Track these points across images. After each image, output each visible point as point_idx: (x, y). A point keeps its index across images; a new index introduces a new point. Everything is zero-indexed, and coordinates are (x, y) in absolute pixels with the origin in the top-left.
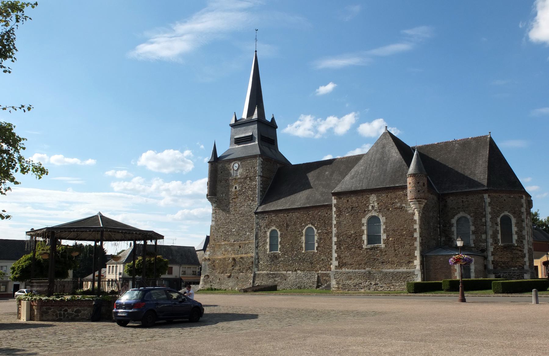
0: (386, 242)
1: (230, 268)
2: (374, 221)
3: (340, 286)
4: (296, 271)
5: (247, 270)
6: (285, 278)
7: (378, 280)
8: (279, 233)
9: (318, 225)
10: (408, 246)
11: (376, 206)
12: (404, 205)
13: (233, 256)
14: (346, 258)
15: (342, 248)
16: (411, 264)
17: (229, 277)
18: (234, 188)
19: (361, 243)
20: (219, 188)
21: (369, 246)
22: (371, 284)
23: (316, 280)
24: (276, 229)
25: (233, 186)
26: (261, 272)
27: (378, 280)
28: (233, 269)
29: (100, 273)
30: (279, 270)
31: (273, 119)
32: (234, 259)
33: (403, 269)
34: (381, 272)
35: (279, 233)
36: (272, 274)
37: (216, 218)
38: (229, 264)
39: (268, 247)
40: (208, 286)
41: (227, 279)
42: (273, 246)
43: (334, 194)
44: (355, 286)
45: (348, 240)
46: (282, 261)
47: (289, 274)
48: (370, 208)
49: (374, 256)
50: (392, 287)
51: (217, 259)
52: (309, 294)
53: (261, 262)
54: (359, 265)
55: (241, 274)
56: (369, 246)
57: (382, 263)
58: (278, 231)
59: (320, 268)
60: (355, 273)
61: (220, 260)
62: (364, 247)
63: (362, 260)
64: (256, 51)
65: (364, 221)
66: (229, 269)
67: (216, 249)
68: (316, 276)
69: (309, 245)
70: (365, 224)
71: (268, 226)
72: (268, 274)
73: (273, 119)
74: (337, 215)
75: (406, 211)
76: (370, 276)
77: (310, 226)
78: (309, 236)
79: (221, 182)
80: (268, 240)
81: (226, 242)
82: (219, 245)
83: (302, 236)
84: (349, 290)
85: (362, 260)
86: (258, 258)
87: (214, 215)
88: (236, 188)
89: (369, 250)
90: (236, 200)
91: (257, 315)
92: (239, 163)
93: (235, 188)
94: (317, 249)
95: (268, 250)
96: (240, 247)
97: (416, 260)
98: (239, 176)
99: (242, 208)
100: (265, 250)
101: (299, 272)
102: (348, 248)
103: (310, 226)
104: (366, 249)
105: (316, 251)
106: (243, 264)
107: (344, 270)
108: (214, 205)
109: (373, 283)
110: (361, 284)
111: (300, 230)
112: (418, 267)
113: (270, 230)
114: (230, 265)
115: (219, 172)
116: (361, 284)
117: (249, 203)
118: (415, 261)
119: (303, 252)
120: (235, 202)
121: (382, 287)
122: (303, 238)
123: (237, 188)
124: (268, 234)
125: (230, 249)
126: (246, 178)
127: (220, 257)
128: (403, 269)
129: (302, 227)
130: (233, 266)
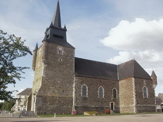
8: (87, 88)
18: (59, 60)
21: (145, 97)
25: (59, 59)
29: (159, 111)
31: (65, 27)
33: (153, 105)
35: (87, 88)
38: (56, 100)
39: (82, 93)
42: (84, 93)
53: (78, 101)
58: (87, 87)
62: (143, 97)
65: (143, 88)
67: (46, 90)
69: (101, 94)
71: (82, 83)
73: (65, 27)
78: (101, 91)
80: (82, 90)
87: (45, 71)
88: (60, 60)
91: (42, 111)
96: (63, 91)
103: (101, 87)
107: (139, 105)
108: (46, 65)
115: (49, 48)
119: (99, 97)
122: (99, 91)
123: (61, 60)
124: (82, 87)
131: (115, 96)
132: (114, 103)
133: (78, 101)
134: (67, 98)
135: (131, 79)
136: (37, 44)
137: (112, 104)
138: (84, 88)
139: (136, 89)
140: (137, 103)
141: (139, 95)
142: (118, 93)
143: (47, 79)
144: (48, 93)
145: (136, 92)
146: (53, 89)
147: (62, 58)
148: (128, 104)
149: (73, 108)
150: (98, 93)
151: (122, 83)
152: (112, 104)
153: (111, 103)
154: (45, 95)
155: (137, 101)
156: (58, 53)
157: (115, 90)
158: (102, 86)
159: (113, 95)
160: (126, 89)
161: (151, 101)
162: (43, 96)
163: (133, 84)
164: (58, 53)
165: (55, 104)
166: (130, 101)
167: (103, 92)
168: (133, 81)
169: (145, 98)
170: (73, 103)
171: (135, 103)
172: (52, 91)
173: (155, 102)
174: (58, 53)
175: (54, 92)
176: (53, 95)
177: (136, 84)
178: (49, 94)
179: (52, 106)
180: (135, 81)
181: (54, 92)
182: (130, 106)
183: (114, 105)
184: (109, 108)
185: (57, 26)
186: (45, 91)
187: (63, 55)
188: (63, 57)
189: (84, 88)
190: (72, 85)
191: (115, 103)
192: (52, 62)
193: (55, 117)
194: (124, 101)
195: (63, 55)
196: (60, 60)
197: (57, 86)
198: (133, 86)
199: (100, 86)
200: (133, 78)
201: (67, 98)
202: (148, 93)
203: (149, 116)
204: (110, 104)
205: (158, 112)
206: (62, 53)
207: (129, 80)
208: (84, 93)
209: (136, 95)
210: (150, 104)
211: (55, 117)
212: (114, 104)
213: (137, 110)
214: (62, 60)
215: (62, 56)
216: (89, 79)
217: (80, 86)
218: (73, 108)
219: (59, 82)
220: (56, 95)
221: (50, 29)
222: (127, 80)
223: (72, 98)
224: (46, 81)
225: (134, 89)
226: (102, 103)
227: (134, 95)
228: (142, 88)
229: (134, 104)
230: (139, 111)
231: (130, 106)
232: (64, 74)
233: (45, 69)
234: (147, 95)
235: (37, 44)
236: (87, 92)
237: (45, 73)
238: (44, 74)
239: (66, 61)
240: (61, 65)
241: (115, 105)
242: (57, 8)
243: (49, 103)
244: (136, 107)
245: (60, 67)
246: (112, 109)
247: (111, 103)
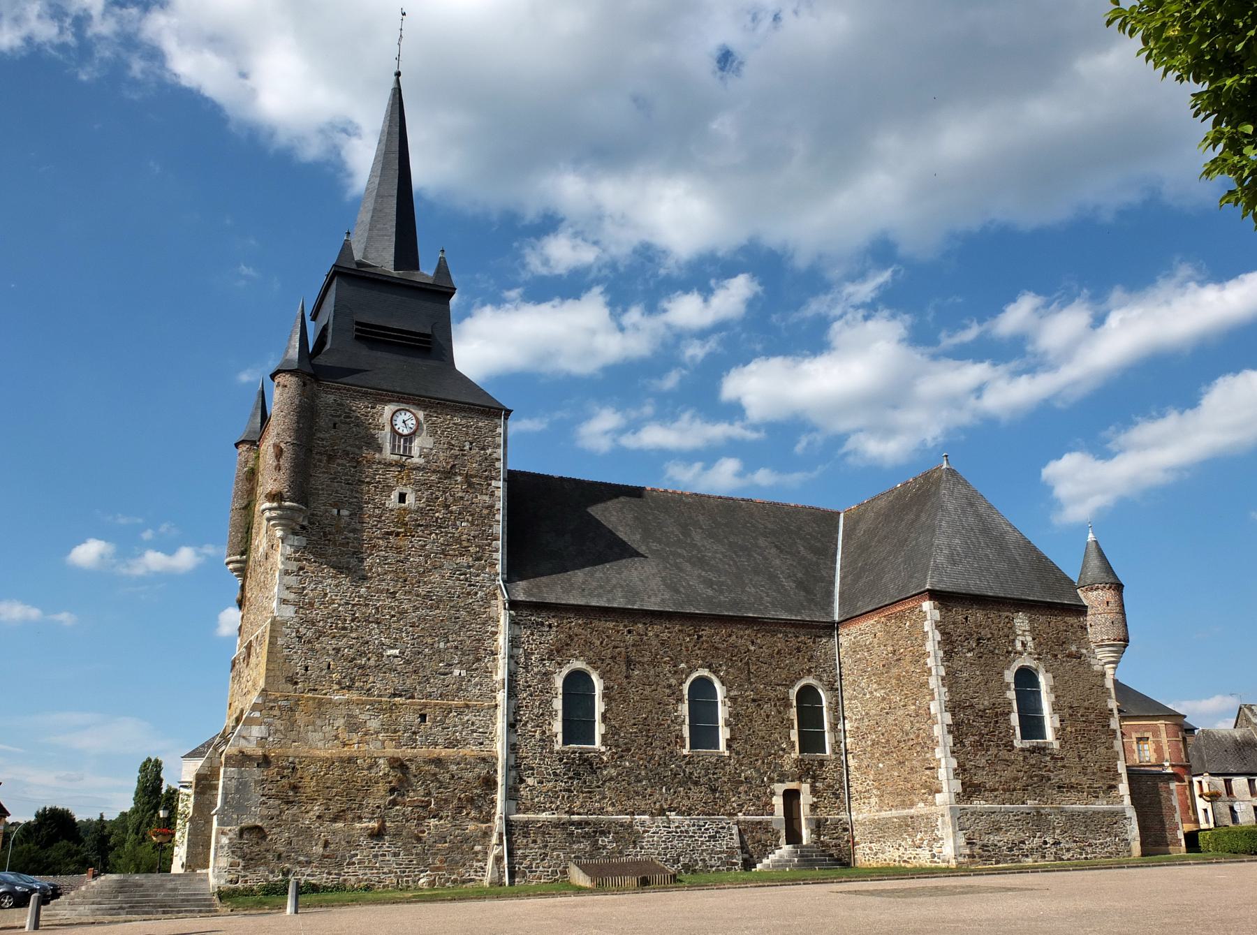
0: (1060, 733)
1: (379, 796)
2: (1026, 678)
3: (977, 850)
4: (662, 812)
5: (459, 809)
6: (629, 835)
7: (1058, 831)
9: (728, 673)
10: (1102, 750)
11: (1030, 644)
12: (1084, 651)
13: (391, 751)
14: (980, 772)
15: (967, 743)
16: (1113, 794)
17: (377, 835)
18: (394, 496)
19: (1007, 735)
20: (320, 479)
21: (1027, 744)
22: (1045, 843)
23: (736, 842)
24: (589, 669)
25: (391, 489)
26: (531, 816)
27: (1058, 831)
28: (394, 803)
30: (601, 811)
32: (399, 765)
33: (1101, 805)
34: (1062, 811)
36: (579, 824)
37: (301, 592)
38: (370, 783)
39: (558, 726)
40: (257, 878)
41: (363, 841)
42: (577, 728)
43: (934, 595)
44: (1011, 849)
45: (980, 723)
46: (611, 779)
47: (642, 823)
48: (1019, 647)
49: (1040, 769)
50: (1089, 850)
51: (314, 760)
52: (718, 885)
53: (530, 781)
54: (1009, 790)
55: (433, 822)
56: (1027, 744)
57: (1059, 787)
59: (741, 806)
60: (1007, 812)
61: (330, 762)
62: (1018, 743)
63: (1016, 779)
64: (398, 74)
65: (1009, 676)
66: (372, 802)
67: (300, 717)
68: (735, 830)
69: (704, 734)
70: (1013, 686)
71: (558, 653)
72: (559, 825)
74: (945, 652)
75: (1090, 665)
76: (1038, 821)
77: (705, 672)
79: (331, 458)
80: (558, 704)
81: (353, 695)
82: (320, 703)
83: (680, 700)
84: (997, 862)
85: (1016, 779)
86: (517, 766)
87: (292, 580)
88: (402, 498)
89: (1027, 754)
90: (404, 543)
92: (421, 415)
93: (402, 498)
94: (729, 747)
95: (560, 737)
96: (423, 717)
97: (1121, 782)
98: (417, 460)
99: (436, 577)
100: (547, 740)
101: (673, 815)
102: (979, 745)
103: (705, 672)
104: (1023, 750)
105: (727, 754)
106: (441, 785)
107: (979, 804)
108: (296, 540)
109: (1051, 841)
110: (1023, 842)
111: (673, 681)
112: (1127, 800)
113: (565, 671)
114: (382, 788)
115: (323, 422)
116: (1023, 842)
117: (463, 561)
118: (1120, 786)
119: (685, 751)
120: (399, 550)
121: (1068, 850)
122: (684, 709)
123: (410, 499)
124: (559, 682)
125: (374, 724)
126: (449, 474)
127: (322, 754)
128: (1101, 805)
129: (680, 675)
130: (392, 790)
131: (812, 741)
132: (805, 788)
133: (530, 781)
134: (453, 767)
135: (912, 610)
136: (397, 93)
137: (791, 797)
138: (577, 687)
139: (950, 680)
140: (970, 790)
141: (974, 729)
142: (837, 708)
143: (309, 634)
144: (314, 737)
145: (953, 707)
146: (348, 702)
147: (416, 482)
148: (905, 797)
149: (494, 840)
150: (677, 721)
151: (858, 642)
152: (791, 797)
153: (780, 788)
154: (295, 750)
155: (961, 770)
156: (387, 447)
157: (808, 694)
158: (715, 672)
159: (801, 734)
160: (889, 678)
161: (1084, 771)
162: (278, 757)
163: (930, 646)
164: (387, 454)
165: (366, 812)
166: (913, 770)
167: (722, 713)
168: (928, 626)
169: (1033, 750)
170: (493, 802)
171: (945, 788)
172: (340, 722)
173: (1117, 775)
174: (387, 454)
175: (353, 727)
176: (346, 752)
177: (949, 645)
178: (319, 744)
179: (340, 825)
180: (938, 625)
181: (353, 727)
182: (920, 808)
183: (805, 811)
184: (765, 827)
185: (384, 259)
186: (293, 723)
187: (422, 461)
188: (419, 476)
189: (577, 687)
190: (488, 673)
191: (814, 791)
192: (345, 512)
193: (290, 909)
194: (879, 773)
195: (422, 461)
196: (402, 498)
197: (380, 684)
198: (930, 662)
199: (692, 669)
200: (927, 605)
201: (453, 767)
202: (1056, 708)
203: (952, 892)
204: (778, 802)
205: (1144, 854)
206: (415, 451)
207: (901, 617)
208: (577, 728)
209: (956, 730)
210: (1073, 795)
211: (290, 909)
212: (806, 799)
213: (970, 843)
214: (418, 499)
215: (418, 469)
216: (611, 625)
217: (547, 676)
218: (494, 840)
219: (396, 652)
220: (373, 747)
221: (335, 282)
222: (889, 618)
223: (489, 761)
224: (300, 649)
225: (934, 682)
226: (714, 790)
227: (938, 731)
228: (1001, 674)
229: (944, 799)
230: (982, 855)
231: (912, 811)
232: (428, 596)
233: (293, 566)
234: (1050, 723)
235: (397, 93)
236: (598, 717)
237: (292, 596)
238: (284, 601)
239: (447, 507)
240: (408, 533)
241: (814, 807)
242: (394, 95)
243: (317, 809)
244: (960, 820)
245: (399, 550)
246: (793, 837)
247: (780, 788)
